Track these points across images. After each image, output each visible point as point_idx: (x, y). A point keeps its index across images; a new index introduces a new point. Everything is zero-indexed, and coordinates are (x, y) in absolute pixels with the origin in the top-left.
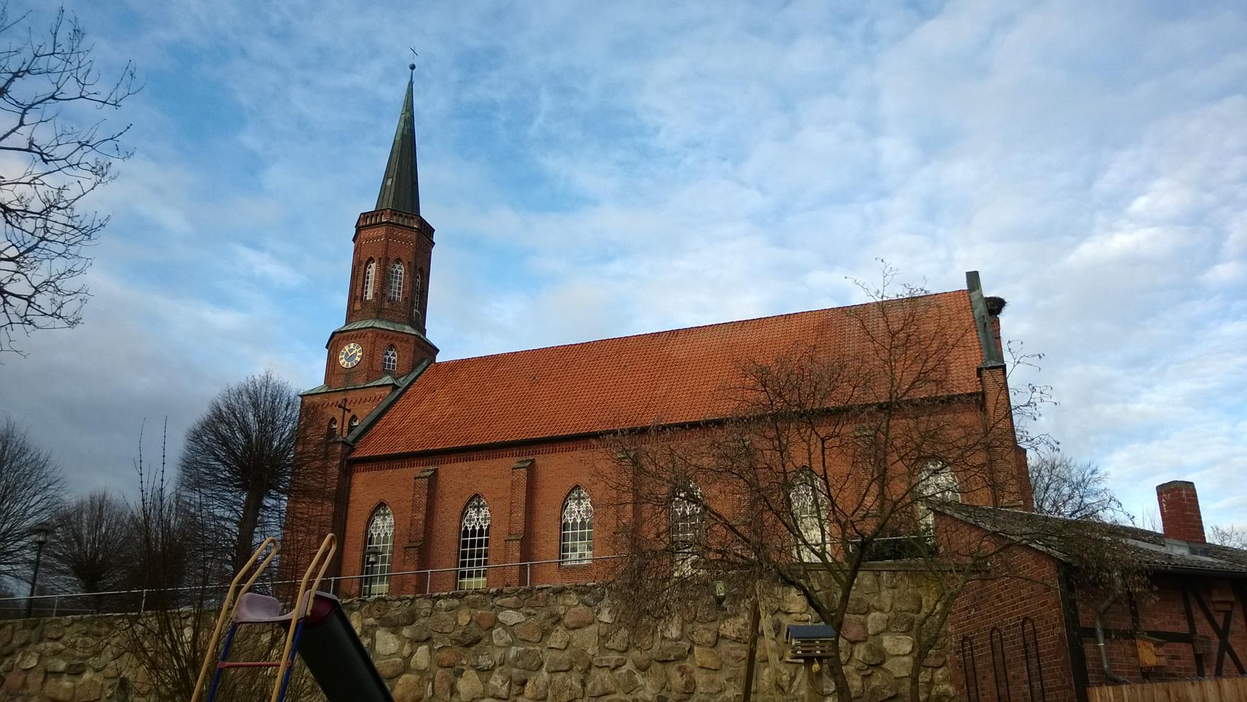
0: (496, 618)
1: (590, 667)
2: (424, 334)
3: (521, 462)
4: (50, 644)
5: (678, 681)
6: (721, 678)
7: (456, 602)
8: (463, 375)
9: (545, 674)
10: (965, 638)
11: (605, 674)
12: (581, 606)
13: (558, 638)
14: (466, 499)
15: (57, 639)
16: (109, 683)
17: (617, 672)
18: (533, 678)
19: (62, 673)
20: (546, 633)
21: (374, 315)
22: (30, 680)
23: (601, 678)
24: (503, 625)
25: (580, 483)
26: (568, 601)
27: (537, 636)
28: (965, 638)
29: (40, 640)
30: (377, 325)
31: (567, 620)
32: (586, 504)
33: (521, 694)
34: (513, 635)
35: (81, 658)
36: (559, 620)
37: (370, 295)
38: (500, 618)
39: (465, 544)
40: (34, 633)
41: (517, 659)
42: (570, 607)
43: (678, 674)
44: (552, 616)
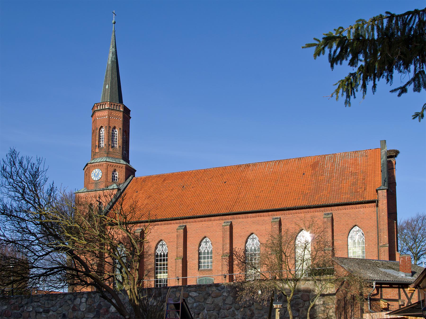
0: (189, 295)
1: (220, 309)
2: (129, 163)
3: (180, 226)
4: (35, 303)
5: (249, 313)
6: (263, 312)
7: (175, 289)
8: (150, 184)
9: (206, 311)
10: (339, 300)
11: (225, 311)
12: (217, 291)
13: (209, 300)
14: (157, 242)
15: (38, 302)
16: (59, 315)
17: (229, 311)
18: (202, 313)
19: (42, 312)
20: (206, 299)
21: (106, 155)
22: (31, 314)
23: (224, 312)
24: (191, 297)
25: (206, 235)
26: (213, 289)
27: (203, 300)
28: (339, 300)
29: (32, 302)
30: (108, 160)
31: (212, 295)
32: (209, 244)
33: (198, 317)
34: (195, 300)
35: (47, 308)
36: (210, 295)
37: (103, 145)
38: (190, 294)
39: (157, 260)
40: (29, 300)
41: (196, 307)
42: (213, 291)
43: (249, 311)
44: (207, 294)
